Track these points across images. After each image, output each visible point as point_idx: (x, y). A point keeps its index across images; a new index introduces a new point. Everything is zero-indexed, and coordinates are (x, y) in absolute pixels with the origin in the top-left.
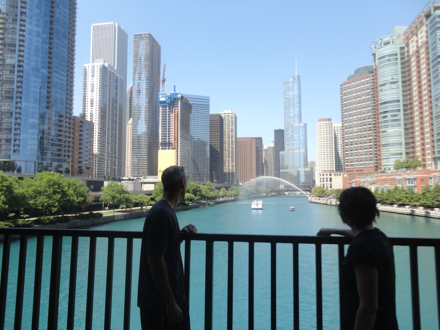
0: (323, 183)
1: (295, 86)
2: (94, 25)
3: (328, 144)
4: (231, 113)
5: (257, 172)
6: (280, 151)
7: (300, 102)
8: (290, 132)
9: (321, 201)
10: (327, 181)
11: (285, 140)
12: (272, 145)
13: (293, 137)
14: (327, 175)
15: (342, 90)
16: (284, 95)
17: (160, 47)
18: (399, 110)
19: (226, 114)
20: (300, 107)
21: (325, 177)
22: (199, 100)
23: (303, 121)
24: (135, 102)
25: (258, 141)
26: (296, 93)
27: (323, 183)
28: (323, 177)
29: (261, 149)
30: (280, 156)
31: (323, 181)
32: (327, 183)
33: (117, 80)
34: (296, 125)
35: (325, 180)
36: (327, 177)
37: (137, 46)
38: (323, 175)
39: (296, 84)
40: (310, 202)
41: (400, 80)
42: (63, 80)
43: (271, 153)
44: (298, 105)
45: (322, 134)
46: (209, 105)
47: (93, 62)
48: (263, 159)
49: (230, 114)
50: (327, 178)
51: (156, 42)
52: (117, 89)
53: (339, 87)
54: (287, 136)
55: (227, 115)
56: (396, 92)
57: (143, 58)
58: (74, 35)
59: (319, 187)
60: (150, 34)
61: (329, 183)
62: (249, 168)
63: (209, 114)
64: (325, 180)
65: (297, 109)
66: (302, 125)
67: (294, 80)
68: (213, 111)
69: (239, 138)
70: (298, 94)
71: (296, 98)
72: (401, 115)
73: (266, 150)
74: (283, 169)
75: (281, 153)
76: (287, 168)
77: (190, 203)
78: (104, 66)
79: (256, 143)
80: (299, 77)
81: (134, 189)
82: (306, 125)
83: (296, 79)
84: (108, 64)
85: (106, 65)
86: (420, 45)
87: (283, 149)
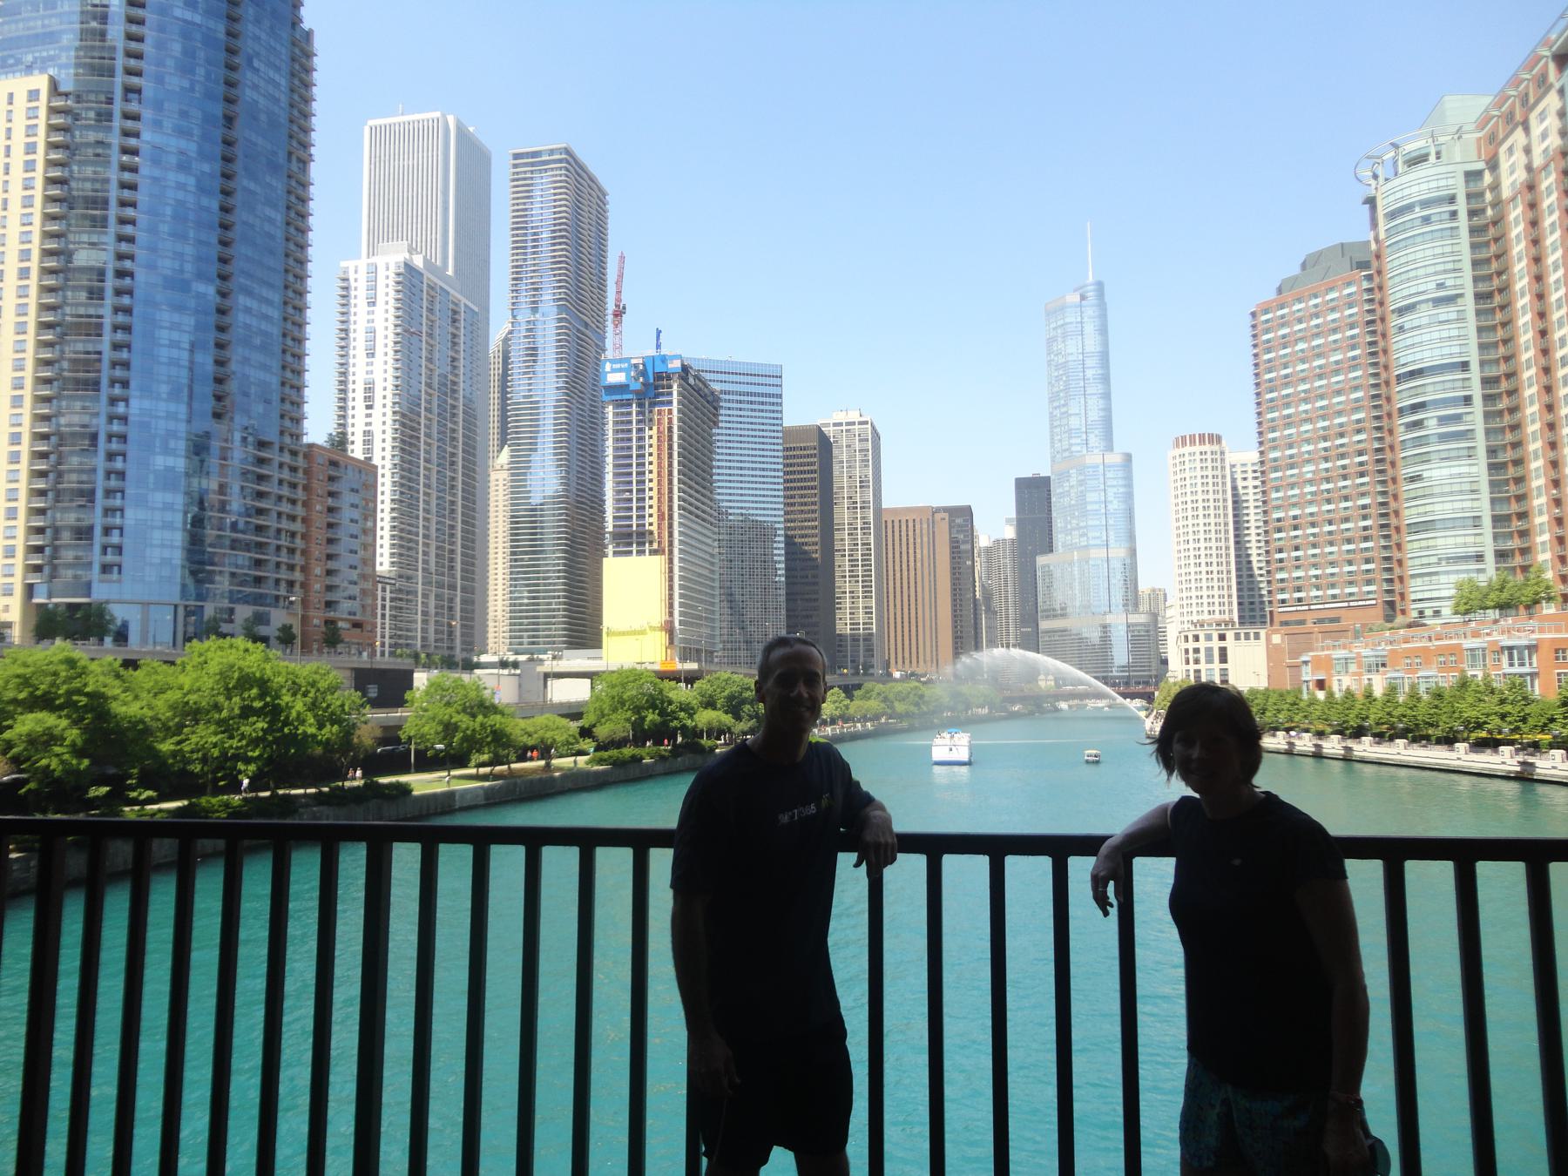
1: (1085, 320)
2: (372, 123)
7: (1106, 379)
8: (1072, 487)
10: (1209, 660)
12: (1010, 533)
14: (1209, 638)
17: (604, 195)
19: (841, 424)
22: (742, 379)
24: (519, 388)
25: (959, 521)
28: (1196, 645)
30: (1039, 573)
31: (1197, 661)
33: (455, 312)
35: (1202, 656)
36: (1209, 644)
37: (523, 191)
38: (1196, 638)
39: (1090, 312)
42: (269, 302)
44: (1100, 386)
46: (780, 396)
47: (372, 252)
49: (857, 427)
50: (1209, 650)
52: (455, 344)
55: (844, 428)
58: (304, 163)
60: (567, 151)
63: (780, 428)
64: (1202, 656)
66: (1114, 458)
67: (1083, 298)
68: (796, 414)
69: (895, 511)
74: (1048, 617)
75: (1041, 560)
78: (409, 267)
79: (951, 527)
80: (1100, 286)
82: (1128, 458)
83: (1091, 295)
84: (426, 260)
85: (418, 261)
86: (1538, 162)
87: (1049, 549)
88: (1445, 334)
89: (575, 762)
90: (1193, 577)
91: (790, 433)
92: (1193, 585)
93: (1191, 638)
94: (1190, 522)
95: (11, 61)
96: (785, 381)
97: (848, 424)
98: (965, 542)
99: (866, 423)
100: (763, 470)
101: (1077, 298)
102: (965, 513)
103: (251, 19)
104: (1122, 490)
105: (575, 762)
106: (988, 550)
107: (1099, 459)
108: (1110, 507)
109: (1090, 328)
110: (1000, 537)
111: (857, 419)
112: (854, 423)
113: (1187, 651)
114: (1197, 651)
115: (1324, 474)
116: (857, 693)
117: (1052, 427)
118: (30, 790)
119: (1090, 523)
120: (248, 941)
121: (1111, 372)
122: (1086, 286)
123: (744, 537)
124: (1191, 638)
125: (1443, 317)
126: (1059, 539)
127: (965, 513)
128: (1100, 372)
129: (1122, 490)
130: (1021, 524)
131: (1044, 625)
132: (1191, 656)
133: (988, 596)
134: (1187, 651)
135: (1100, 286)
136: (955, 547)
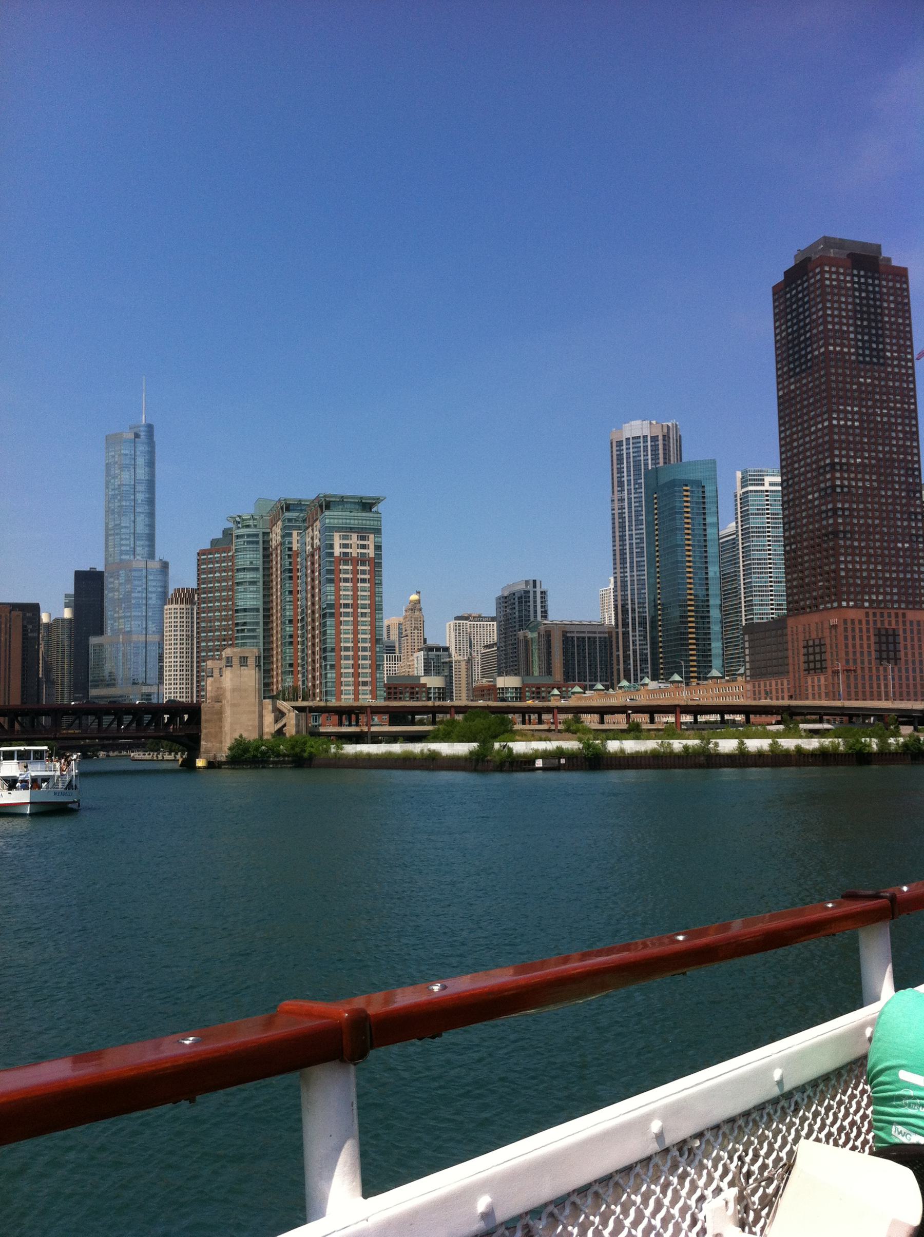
1: (138, 453)
3: (173, 664)
7: (151, 502)
8: (120, 584)
11: (106, 604)
13: (128, 597)
15: (200, 563)
16: (107, 476)
18: (257, 624)
20: (151, 515)
23: (159, 554)
26: (142, 473)
29: (35, 635)
30: (91, 651)
34: (139, 562)
39: (142, 448)
41: (261, 580)
43: (64, 638)
44: (147, 507)
45: (173, 629)
48: (41, 662)
53: (195, 557)
54: (113, 591)
56: (255, 596)
59: (900, 733)
65: (141, 521)
66: (154, 565)
67: (137, 436)
70: (147, 478)
71: (140, 488)
72: (260, 630)
73: (48, 626)
74: (96, 686)
75: (94, 640)
76: (114, 685)
77: (277, 688)
79: (23, 619)
80: (150, 428)
82: (165, 566)
83: (143, 434)
87: (100, 631)
88: (252, 596)
89: (602, 722)
92: (172, 682)
94: (173, 647)
98: (32, 631)
101: (132, 436)
104: (159, 589)
105: (602, 722)
107: (143, 565)
108: (150, 602)
109: (141, 461)
115: (223, 637)
117: (107, 536)
118: (734, 720)
119: (133, 614)
120: (206, 721)
121: (157, 496)
122: (139, 427)
125: (251, 589)
128: (147, 496)
129: (159, 589)
133: (48, 670)
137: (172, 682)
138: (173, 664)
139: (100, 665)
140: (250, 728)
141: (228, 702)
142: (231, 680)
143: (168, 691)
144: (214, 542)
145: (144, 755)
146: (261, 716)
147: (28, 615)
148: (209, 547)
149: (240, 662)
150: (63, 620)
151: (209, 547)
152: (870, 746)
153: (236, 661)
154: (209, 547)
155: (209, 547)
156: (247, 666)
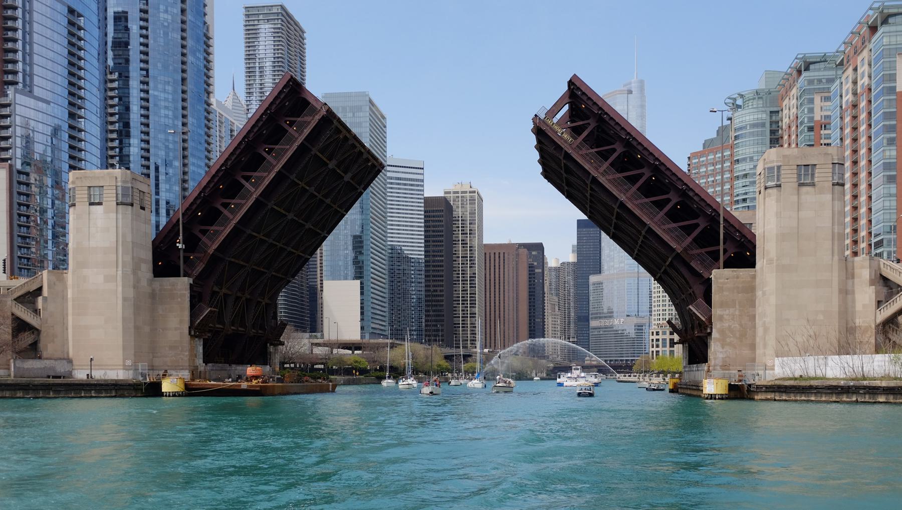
0: (657, 349)
1: (630, 107)
4: (470, 192)
5: (19, 297)
6: (591, 274)
9: (632, 377)
10: (664, 346)
12: (571, 258)
14: (664, 333)
17: (303, 32)
19: (457, 192)
21: (660, 337)
27: (657, 349)
28: (658, 337)
32: (664, 349)
35: (660, 343)
36: (664, 337)
37: (251, 35)
38: (657, 334)
40: (619, 382)
46: (422, 181)
49: (468, 194)
51: (296, 24)
55: (460, 195)
57: (268, 64)
60: (282, 7)
61: (668, 349)
62: (511, 275)
63: (422, 197)
64: (660, 343)
68: (432, 190)
75: (593, 279)
80: (641, 83)
81: (186, 369)
87: (598, 270)
90: (661, 299)
91: (429, 202)
92: (661, 303)
93: (655, 333)
95: (657, 456)
96: (426, 171)
97: (462, 192)
99: (474, 192)
100: (398, 209)
102: (539, 247)
103: (162, 11)
106: (557, 270)
110: (566, 260)
111: (468, 189)
112: (466, 192)
113: (653, 340)
114: (658, 340)
116: (469, 359)
123: (400, 268)
124: (655, 333)
126: (605, 265)
127: (539, 247)
130: (580, 249)
131: (593, 323)
132: (655, 343)
134: (653, 340)
135: (641, 83)
136: (531, 268)
137: (661, 303)
138: (661, 312)
139: (599, 302)
140: (821, 317)
141: (770, 261)
142: (778, 215)
143: (656, 299)
144: (708, 144)
145: (625, 376)
146: (846, 292)
147: (534, 253)
148: (701, 149)
149: (799, 176)
150: (568, 263)
151: (702, 149)
152: (42, 394)
153: (789, 177)
154: (702, 149)
155: (701, 149)
156: (813, 185)
